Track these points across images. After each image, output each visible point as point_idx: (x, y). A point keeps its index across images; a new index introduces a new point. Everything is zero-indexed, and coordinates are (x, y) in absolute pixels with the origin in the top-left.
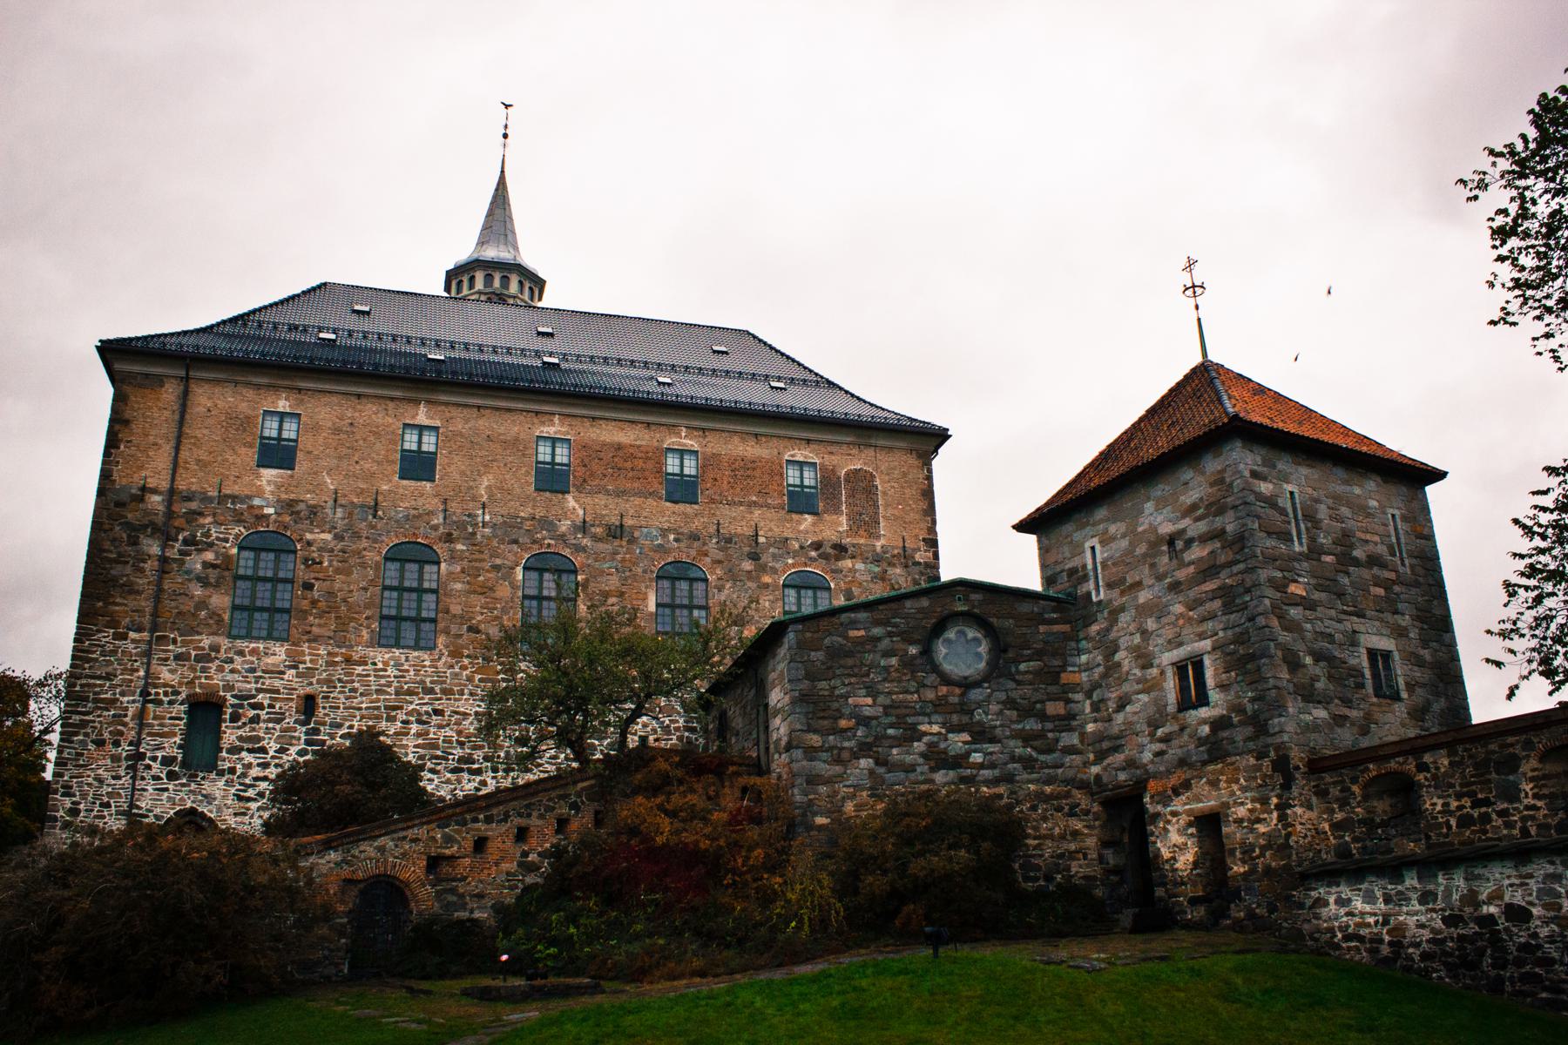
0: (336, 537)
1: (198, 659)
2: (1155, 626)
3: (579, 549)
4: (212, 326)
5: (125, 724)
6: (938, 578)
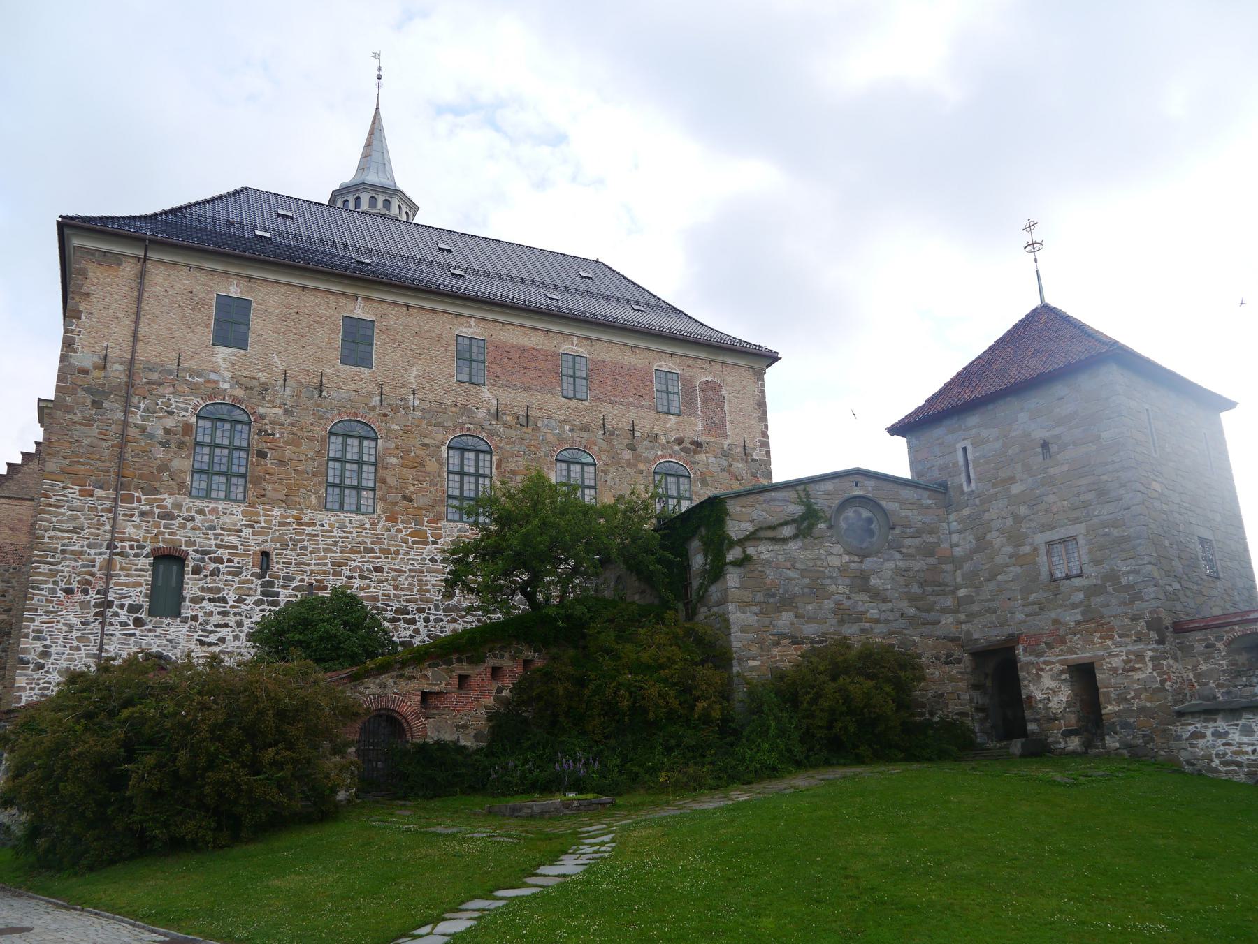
0: (286, 411)
1: (161, 517)
2: (1027, 512)
3: (493, 434)
4: (156, 215)
5: (92, 574)
6: (769, 475)
